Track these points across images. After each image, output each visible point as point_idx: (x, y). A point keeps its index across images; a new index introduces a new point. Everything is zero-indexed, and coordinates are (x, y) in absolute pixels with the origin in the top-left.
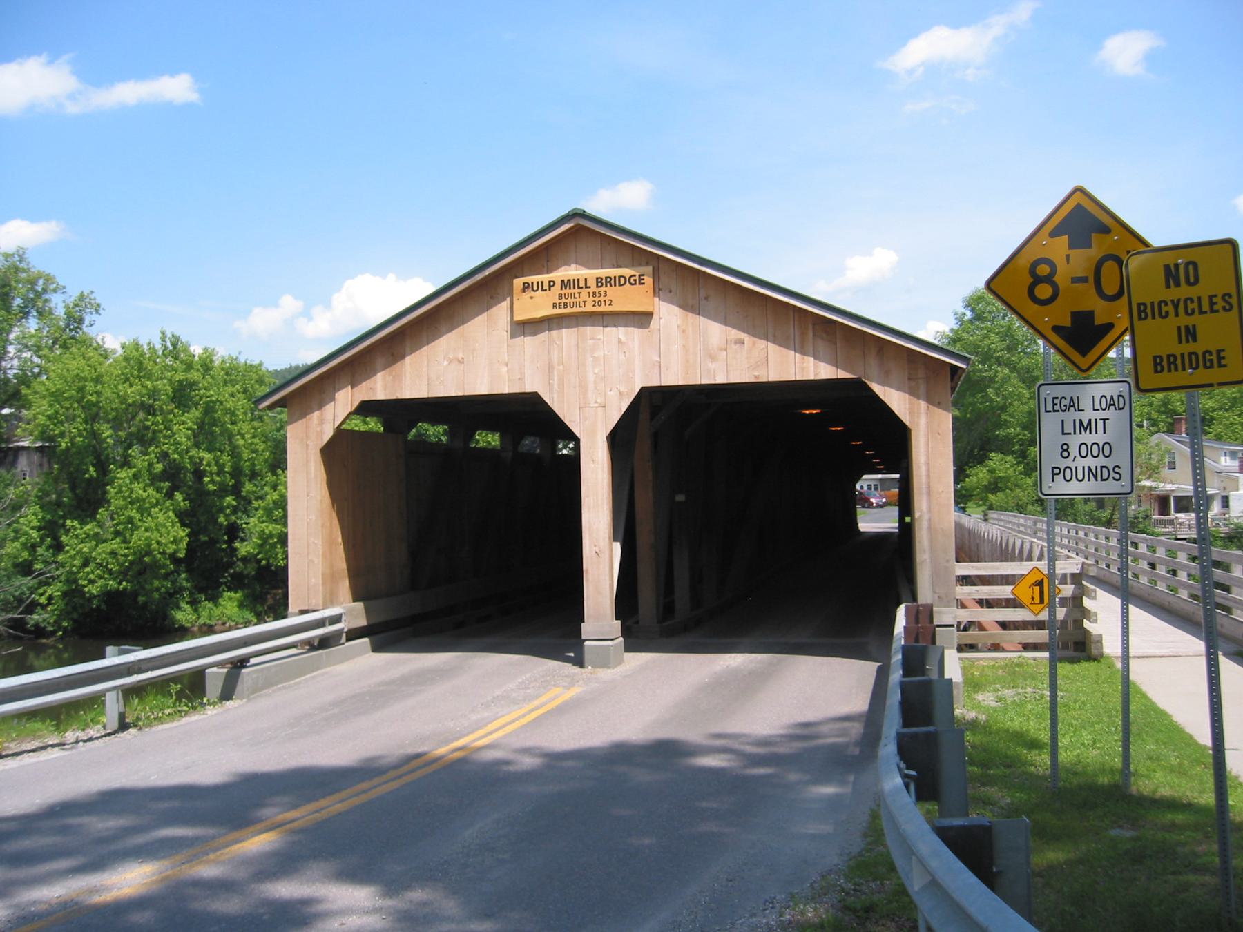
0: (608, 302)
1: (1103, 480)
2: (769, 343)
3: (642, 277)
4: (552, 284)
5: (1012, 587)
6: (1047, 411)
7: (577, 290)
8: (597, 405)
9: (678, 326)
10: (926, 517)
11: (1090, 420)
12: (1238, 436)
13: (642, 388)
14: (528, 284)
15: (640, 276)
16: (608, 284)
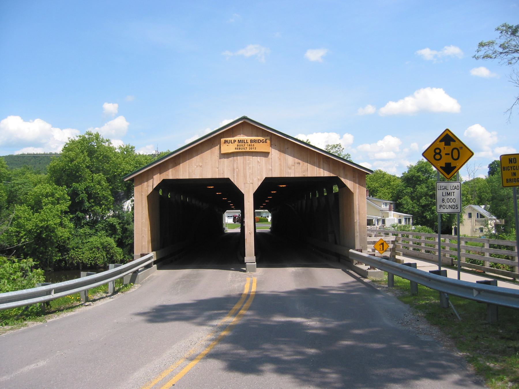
0: (255, 148)
1: (453, 209)
2: (308, 164)
3: (266, 140)
4: (235, 141)
5: (374, 245)
6: (438, 190)
7: (244, 144)
8: (250, 183)
9: (278, 157)
10: (358, 221)
11: (450, 192)
12: (387, 197)
13: (266, 177)
14: (226, 141)
15: (265, 140)
16: (255, 142)
